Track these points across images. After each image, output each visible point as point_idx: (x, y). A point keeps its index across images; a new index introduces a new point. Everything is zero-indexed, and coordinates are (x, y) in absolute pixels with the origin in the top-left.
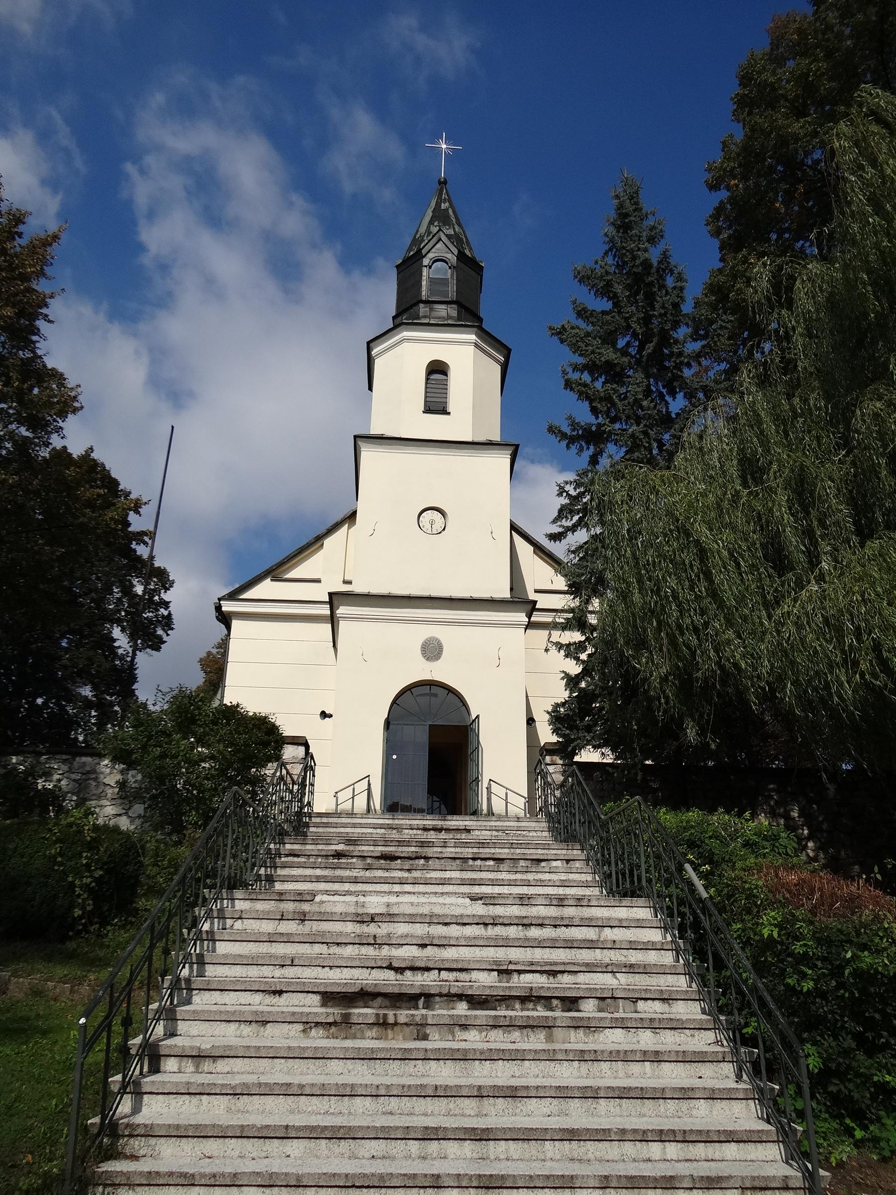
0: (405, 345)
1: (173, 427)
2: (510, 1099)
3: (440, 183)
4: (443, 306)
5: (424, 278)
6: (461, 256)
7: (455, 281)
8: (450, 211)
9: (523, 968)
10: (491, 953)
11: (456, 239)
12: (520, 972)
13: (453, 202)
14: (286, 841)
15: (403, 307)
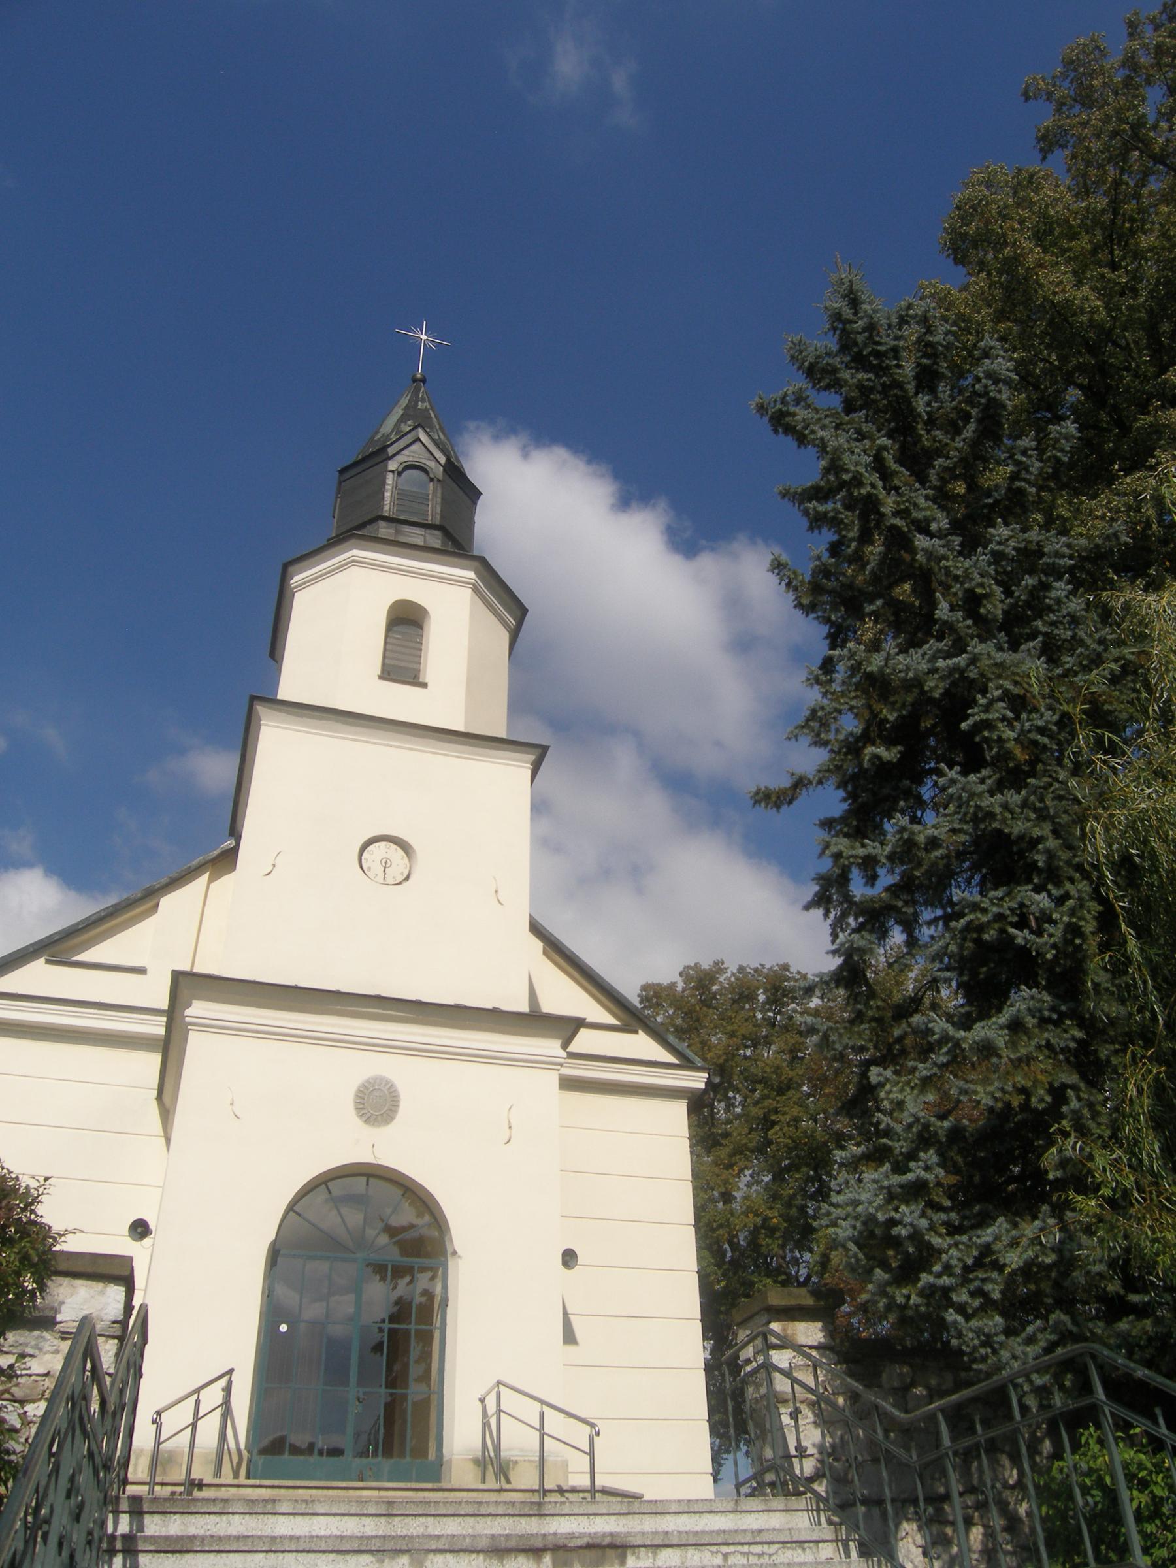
7: (439, 500)
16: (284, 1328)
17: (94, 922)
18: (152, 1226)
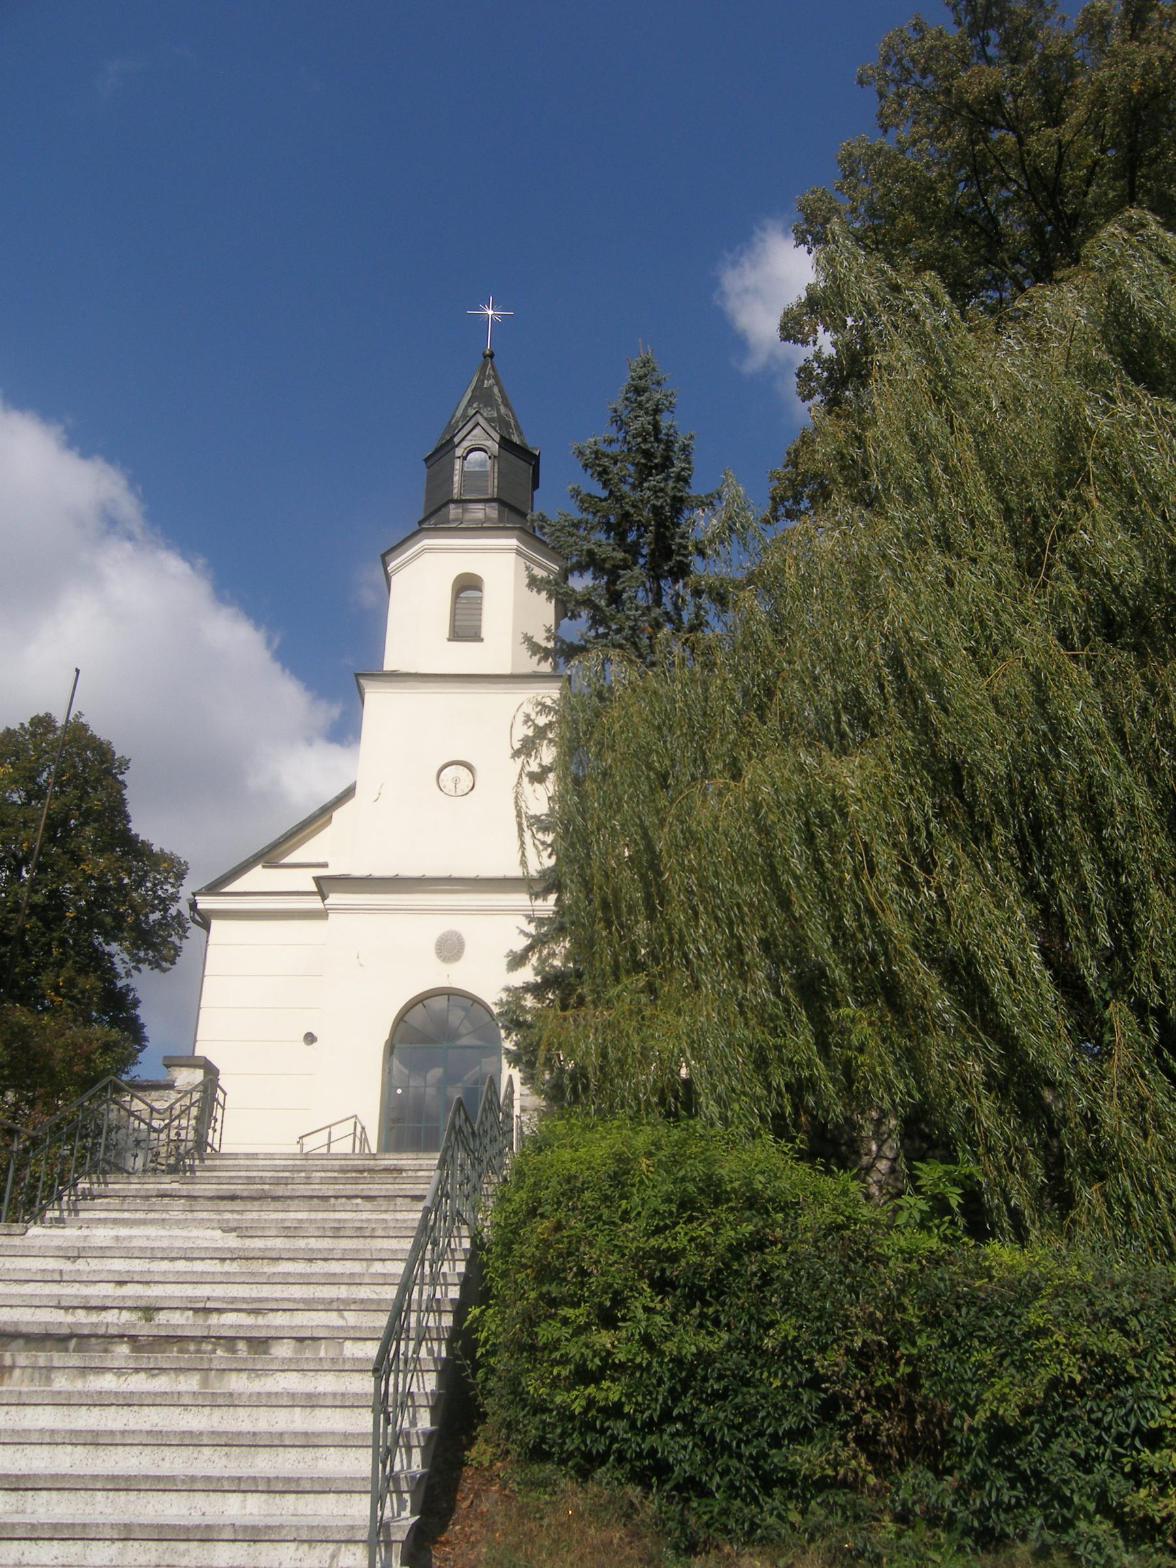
0: (427, 556)
1: (78, 671)
2: (91, 1447)
3: (485, 356)
4: (481, 506)
5: (456, 472)
6: (506, 443)
8: (496, 390)
9: (224, 1306)
10: (189, 1291)
11: (501, 423)
12: (219, 1311)
14: (108, 1180)
15: (431, 510)
16: (399, 1091)
18: (315, 1034)
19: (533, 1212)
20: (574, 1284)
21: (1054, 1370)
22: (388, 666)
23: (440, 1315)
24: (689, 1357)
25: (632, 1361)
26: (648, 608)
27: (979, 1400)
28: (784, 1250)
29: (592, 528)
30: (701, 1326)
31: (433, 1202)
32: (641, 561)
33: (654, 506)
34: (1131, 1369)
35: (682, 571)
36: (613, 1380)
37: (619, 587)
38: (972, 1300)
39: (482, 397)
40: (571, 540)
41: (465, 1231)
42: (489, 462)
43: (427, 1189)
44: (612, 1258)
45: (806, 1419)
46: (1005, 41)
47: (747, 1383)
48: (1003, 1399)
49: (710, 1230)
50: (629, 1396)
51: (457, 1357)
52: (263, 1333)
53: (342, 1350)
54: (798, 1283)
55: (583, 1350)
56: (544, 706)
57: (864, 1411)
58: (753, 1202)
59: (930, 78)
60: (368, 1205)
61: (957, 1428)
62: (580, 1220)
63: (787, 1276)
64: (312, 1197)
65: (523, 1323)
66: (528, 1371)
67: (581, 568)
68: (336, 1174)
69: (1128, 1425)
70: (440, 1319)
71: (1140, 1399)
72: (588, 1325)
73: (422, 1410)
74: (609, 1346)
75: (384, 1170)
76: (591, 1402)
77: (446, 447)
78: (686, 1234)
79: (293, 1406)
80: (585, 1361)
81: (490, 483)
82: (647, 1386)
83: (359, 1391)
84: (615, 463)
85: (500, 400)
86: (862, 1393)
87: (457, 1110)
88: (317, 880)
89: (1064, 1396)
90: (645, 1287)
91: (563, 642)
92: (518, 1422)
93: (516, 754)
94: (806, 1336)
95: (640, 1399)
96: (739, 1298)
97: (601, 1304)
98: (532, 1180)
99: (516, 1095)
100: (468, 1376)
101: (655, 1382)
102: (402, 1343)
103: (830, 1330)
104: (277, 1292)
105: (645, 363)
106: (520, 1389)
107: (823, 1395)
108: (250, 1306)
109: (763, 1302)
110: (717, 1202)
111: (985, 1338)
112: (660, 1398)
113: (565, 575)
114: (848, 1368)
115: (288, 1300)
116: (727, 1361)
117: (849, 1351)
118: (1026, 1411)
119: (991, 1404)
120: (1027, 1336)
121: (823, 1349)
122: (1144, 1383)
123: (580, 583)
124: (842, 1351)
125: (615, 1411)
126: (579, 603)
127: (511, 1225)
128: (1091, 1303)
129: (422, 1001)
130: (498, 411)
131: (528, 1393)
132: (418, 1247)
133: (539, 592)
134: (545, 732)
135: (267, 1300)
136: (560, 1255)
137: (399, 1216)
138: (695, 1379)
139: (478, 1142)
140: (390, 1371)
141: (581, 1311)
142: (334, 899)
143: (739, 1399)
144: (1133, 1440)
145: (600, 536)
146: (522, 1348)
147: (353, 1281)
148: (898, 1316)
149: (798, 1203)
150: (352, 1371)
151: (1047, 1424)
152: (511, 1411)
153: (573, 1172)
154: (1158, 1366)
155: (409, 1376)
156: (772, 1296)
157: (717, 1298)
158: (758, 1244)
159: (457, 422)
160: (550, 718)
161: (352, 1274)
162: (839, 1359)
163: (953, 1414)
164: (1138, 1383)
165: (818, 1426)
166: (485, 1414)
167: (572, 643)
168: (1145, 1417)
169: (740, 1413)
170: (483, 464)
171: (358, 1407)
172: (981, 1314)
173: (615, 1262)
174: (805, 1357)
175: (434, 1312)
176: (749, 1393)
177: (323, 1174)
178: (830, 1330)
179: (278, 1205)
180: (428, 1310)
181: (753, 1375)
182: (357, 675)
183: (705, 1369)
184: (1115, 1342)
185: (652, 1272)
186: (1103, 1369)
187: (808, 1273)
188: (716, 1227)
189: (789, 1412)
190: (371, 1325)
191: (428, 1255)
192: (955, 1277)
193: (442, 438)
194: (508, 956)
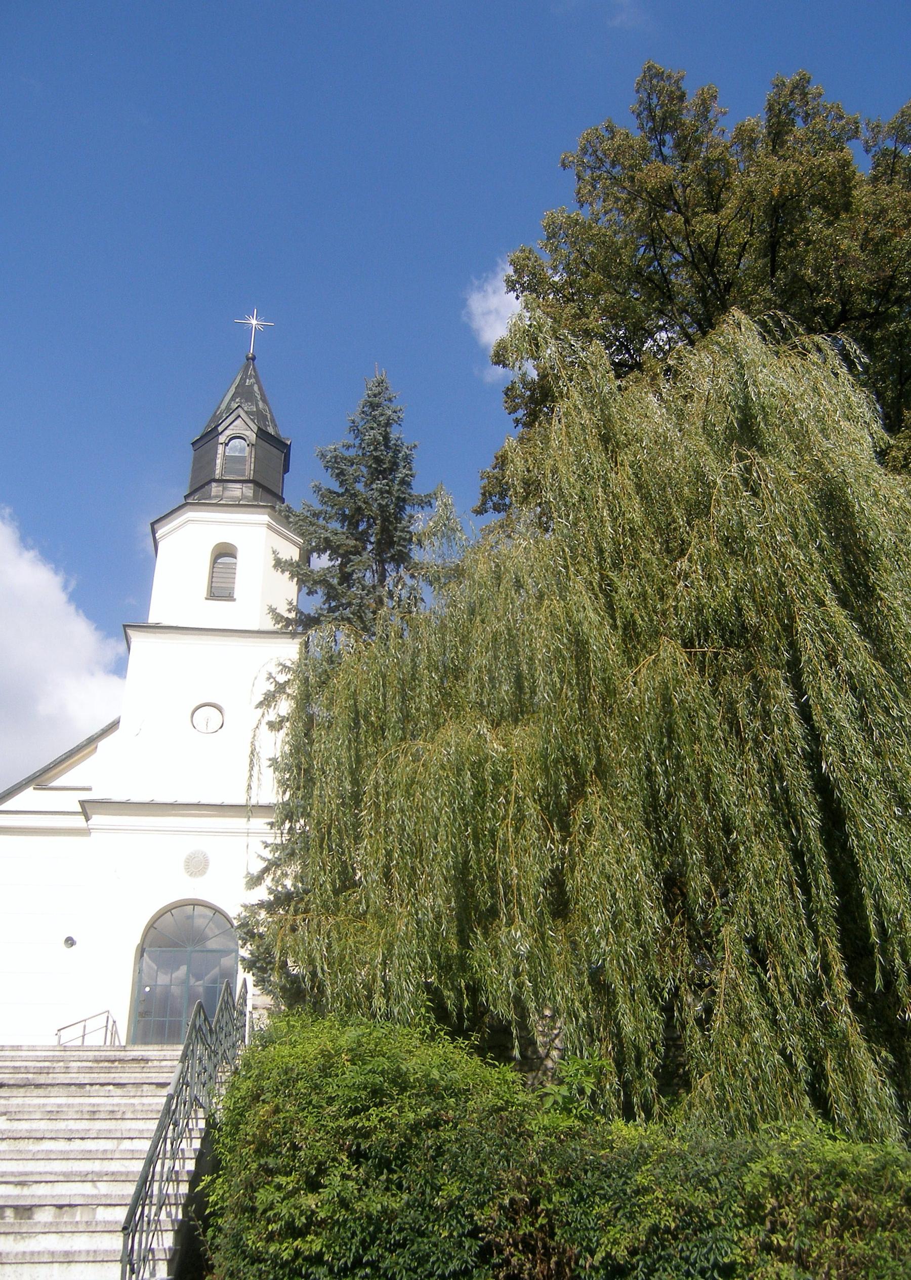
0: (190, 527)
4: (238, 486)
6: (262, 434)
8: (256, 388)
11: (259, 416)
13: (261, 379)
17: (60, 762)
18: (75, 939)
19: (256, 1098)
20: (287, 1157)
21: (654, 1219)
22: (152, 619)
23: (178, 1184)
24: (375, 1213)
25: (331, 1218)
26: (374, 587)
27: (599, 1244)
28: (455, 1127)
29: (330, 518)
30: (387, 1189)
31: (176, 1091)
32: (370, 547)
33: (379, 504)
34: (711, 1217)
35: (402, 559)
36: (317, 1234)
37: (348, 570)
38: (596, 1167)
39: (244, 393)
40: (312, 529)
41: (201, 1113)
42: (247, 448)
43: (172, 1078)
44: (318, 1136)
45: (467, 1262)
46: (677, 145)
47: (422, 1234)
48: (615, 1242)
49: (396, 1112)
50: (328, 1247)
51: (191, 1219)
52: (28, 1202)
53: (94, 1215)
54: (464, 1154)
55: (292, 1211)
56: (285, 666)
57: (512, 1255)
58: (433, 1090)
59: (618, 168)
60: (119, 1091)
61: (581, 1267)
62: (294, 1105)
63: (454, 1149)
64: (70, 1085)
65: (246, 1189)
66: (248, 1228)
67: (320, 551)
68: (90, 1064)
69: (708, 1261)
70: (178, 1187)
71: (717, 1240)
72: (295, 1191)
73: (161, 1262)
74: (314, 1206)
75: (133, 1060)
76: (297, 1253)
77: (210, 436)
78: (377, 1115)
79: (52, 1262)
80: (294, 1220)
81: (247, 467)
82: (343, 1239)
83: (109, 1248)
84: (352, 465)
85: (259, 397)
86: (511, 1240)
87: (198, 1013)
88: (82, 803)
89: (662, 1240)
90: (344, 1158)
91: (302, 613)
92: (239, 1271)
93: (260, 705)
94: (468, 1196)
95: (337, 1249)
96: (417, 1166)
97: (307, 1173)
98: (257, 1072)
99: (249, 996)
100: (199, 1235)
101: (349, 1235)
102: (147, 1208)
103: (486, 1191)
104: (41, 1166)
105: (380, 383)
106: (242, 1243)
107: (480, 1243)
108: (17, 1179)
109: (437, 1170)
110: (403, 1090)
111: (605, 1195)
112: (354, 1248)
113: (306, 557)
114: (501, 1221)
115: (51, 1173)
116: (406, 1216)
117: (501, 1207)
118: (633, 1252)
119: (606, 1246)
120: (637, 1192)
121: (481, 1206)
122: (721, 1229)
123: (322, 562)
124: (496, 1208)
125: (317, 1259)
126: (315, 583)
127: (239, 1108)
128: (685, 1167)
129: (170, 910)
130: (257, 406)
131: (247, 1246)
132: (162, 1128)
133: (283, 572)
134: (284, 688)
135: (32, 1173)
136: (277, 1134)
137: (145, 1100)
138: (382, 1232)
139: (214, 1038)
140: (136, 1231)
141: (292, 1178)
142: (97, 820)
143: (415, 1248)
144: (712, 1272)
145: (335, 525)
146: (244, 1210)
147: (105, 1157)
148: (539, 1179)
149: (468, 1090)
150: (103, 1232)
151: (649, 1261)
152: (233, 1263)
153: (290, 1065)
154: (731, 1215)
155: (151, 1234)
156: (443, 1164)
157: (400, 1167)
158: (435, 1123)
159: (221, 413)
160: (289, 676)
161: (105, 1151)
162: (494, 1214)
163: (579, 1256)
164: (716, 1228)
165: (477, 1267)
166: (213, 1266)
167: (309, 614)
168: (721, 1254)
169: (416, 1259)
170: (242, 450)
171: (107, 1261)
172: (602, 1177)
173: (321, 1139)
174: (467, 1213)
175: (173, 1181)
176: (423, 1242)
177: (79, 1064)
178: (486, 1191)
179: (41, 1092)
180: (168, 1180)
181: (427, 1228)
182: (125, 626)
183: (389, 1223)
184: (699, 1199)
185: (351, 1146)
186: (691, 1218)
187: (472, 1146)
188: (401, 1109)
189: (454, 1257)
190: (120, 1193)
191: (170, 1134)
192: (584, 1148)
193: (208, 426)
194: (246, 877)
